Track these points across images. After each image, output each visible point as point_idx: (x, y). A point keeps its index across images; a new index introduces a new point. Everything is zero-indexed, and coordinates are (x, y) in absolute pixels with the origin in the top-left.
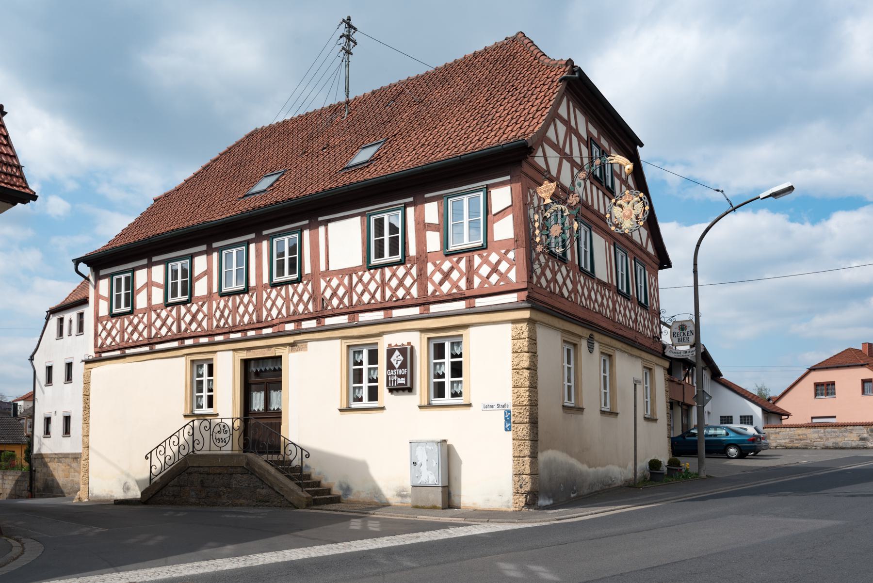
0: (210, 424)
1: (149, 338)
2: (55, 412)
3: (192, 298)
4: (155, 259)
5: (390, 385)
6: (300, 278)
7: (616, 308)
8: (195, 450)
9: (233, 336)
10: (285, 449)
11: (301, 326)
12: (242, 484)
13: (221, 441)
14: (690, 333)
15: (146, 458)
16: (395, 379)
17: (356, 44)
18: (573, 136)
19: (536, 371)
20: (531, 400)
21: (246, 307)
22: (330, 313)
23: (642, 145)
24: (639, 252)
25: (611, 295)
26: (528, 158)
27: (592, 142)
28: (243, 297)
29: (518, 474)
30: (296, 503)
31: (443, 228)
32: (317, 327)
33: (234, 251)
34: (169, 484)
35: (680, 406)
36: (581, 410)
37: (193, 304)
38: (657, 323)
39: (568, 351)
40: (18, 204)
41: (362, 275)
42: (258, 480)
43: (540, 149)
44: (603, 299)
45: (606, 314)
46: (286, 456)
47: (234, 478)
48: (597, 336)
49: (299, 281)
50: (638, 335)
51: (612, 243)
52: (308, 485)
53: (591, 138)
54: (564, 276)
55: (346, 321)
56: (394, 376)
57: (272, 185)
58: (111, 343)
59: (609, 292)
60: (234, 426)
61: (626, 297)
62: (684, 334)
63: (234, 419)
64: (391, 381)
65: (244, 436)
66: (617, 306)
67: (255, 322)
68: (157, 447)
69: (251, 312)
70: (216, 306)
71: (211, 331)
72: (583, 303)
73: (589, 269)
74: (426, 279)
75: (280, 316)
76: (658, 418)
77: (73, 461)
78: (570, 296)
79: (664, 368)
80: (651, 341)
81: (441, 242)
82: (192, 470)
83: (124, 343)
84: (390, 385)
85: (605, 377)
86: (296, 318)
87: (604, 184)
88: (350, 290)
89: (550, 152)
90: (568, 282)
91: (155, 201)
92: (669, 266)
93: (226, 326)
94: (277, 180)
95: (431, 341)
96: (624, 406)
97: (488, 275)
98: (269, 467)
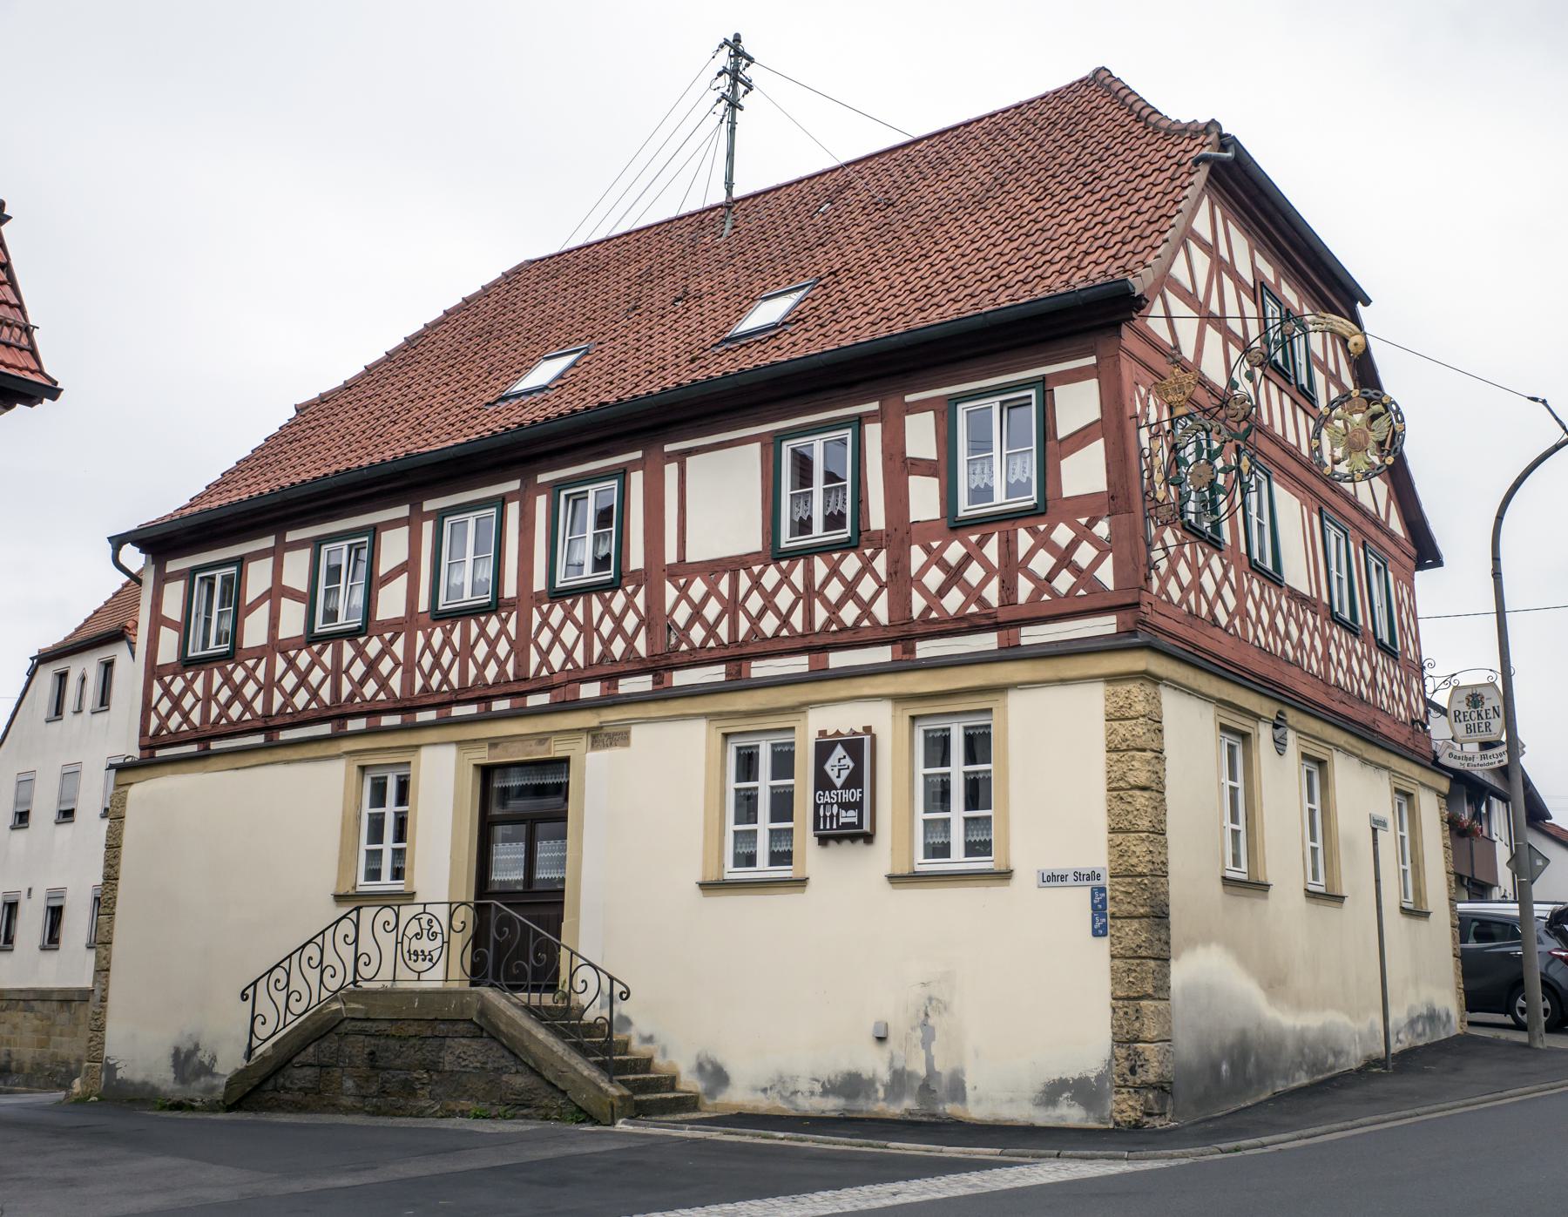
0: (397, 916)
1: (267, 715)
2: (30, 890)
3: (370, 624)
4: (291, 536)
5: (822, 827)
6: (618, 580)
7: (1330, 654)
8: (358, 978)
9: (457, 711)
10: (571, 976)
11: (616, 688)
12: (466, 1063)
13: (420, 958)
14: (1491, 714)
15: (244, 996)
16: (835, 813)
17: (750, 88)
18: (1225, 276)
19: (1162, 793)
20: (1153, 863)
21: (493, 644)
22: (686, 658)
23: (1367, 302)
24: (1372, 531)
25: (1318, 624)
26: (1134, 319)
27: (1264, 291)
28: (487, 622)
29: (1124, 1040)
30: (594, 1109)
31: (944, 469)
32: (654, 691)
33: (471, 519)
34: (294, 1061)
35: (1464, 886)
36: (1263, 887)
37: (371, 637)
38: (1419, 689)
39: (1231, 748)
40: (18, 405)
41: (762, 573)
42: (506, 1054)
43: (1158, 302)
44: (1301, 632)
45: (1310, 666)
46: (573, 996)
47: (449, 1047)
48: (1292, 716)
49: (614, 586)
50: (1379, 716)
51: (1316, 509)
52: (624, 1067)
53: (1262, 284)
54: (1218, 578)
55: (722, 678)
56: (832, 804)
57: (561, 376)
58: (180, 725)
59: (1313, 618)
60: (453, 922)
61: (1351, 628)
62: (1479, 715)
63: (454, 906)
64: (825, 816)
65: (474, 948)
66: (1333, 650)
67: (512, 679)
68: (271, 971)
69: (502, 657)
70: (423, 641)
71: (409, 700)
72: (1259, 642)
73: (1269, 565)
74: (909, 582)
75: (569, 666)
76: (1430, 910)
77: (62, 1007)
78: (1230, 623)
79: (1439, 793)
80: (1406, 731)
81: (941, 499)
82: (348, 1026)
83: (208, 727)
84: (822, 827)
85: (1312, 811)
86: (606, 669)
87: (1293, 381)
88: (733, 606)
89: (1178, 307)
90: (1227, 591)
91: (297, 411)
92: (1438, 562)
93: (445, 688)
94: (574, 365)
95: (918, 723)
96: (1355, 879)
97: (1049, 574)
98: (528, 1023)
